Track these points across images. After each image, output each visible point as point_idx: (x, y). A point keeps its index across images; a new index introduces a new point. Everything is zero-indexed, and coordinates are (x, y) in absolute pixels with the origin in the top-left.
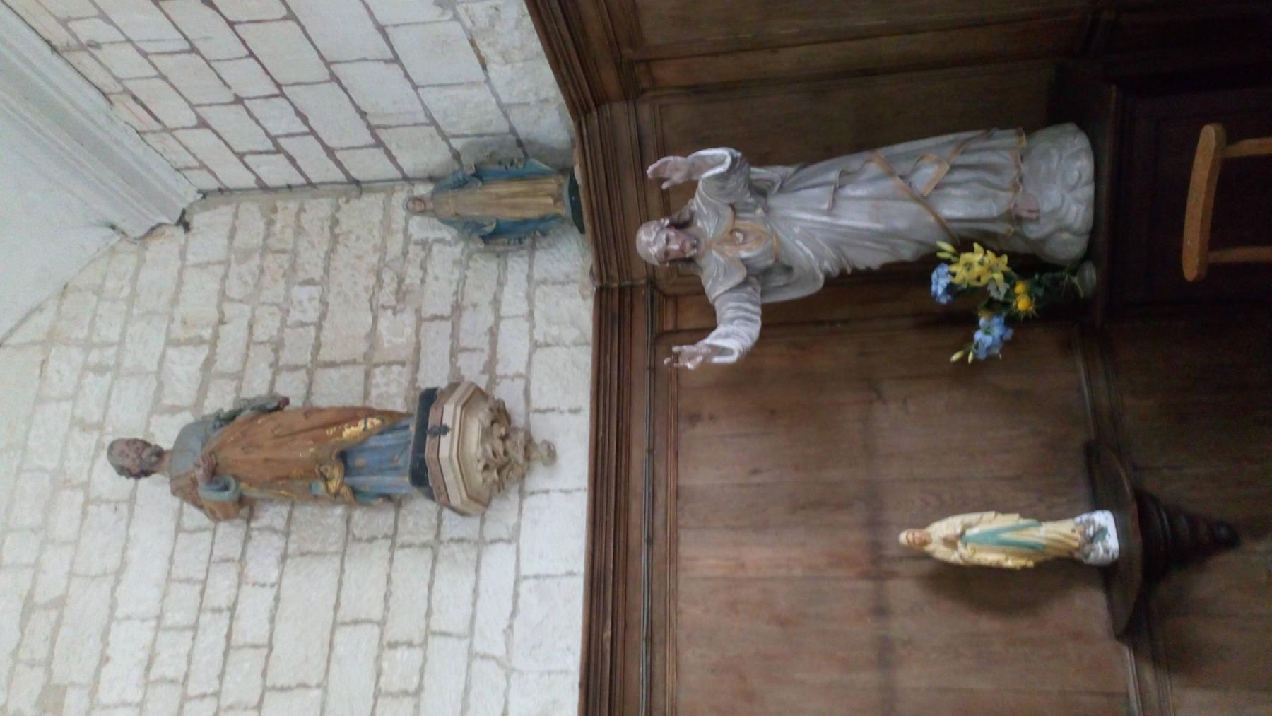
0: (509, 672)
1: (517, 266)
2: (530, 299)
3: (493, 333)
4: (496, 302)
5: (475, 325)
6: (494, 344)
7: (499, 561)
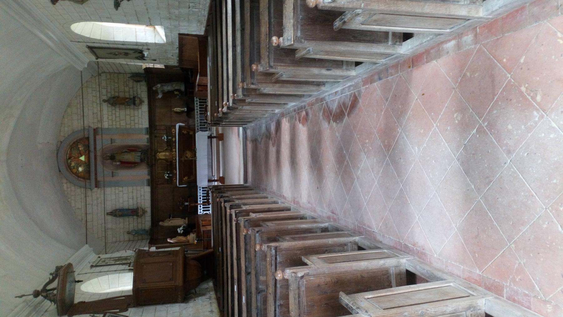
0: (142, 119)
1: (139, 84)
2: (140, 86)
3: (137, 90)
4: (137, 87)
5: (135, 89)
6: (137, 91)
7: (140, 111)
